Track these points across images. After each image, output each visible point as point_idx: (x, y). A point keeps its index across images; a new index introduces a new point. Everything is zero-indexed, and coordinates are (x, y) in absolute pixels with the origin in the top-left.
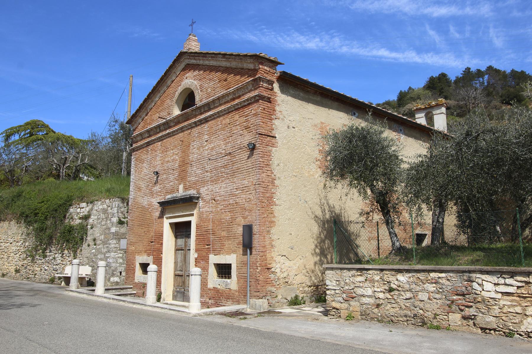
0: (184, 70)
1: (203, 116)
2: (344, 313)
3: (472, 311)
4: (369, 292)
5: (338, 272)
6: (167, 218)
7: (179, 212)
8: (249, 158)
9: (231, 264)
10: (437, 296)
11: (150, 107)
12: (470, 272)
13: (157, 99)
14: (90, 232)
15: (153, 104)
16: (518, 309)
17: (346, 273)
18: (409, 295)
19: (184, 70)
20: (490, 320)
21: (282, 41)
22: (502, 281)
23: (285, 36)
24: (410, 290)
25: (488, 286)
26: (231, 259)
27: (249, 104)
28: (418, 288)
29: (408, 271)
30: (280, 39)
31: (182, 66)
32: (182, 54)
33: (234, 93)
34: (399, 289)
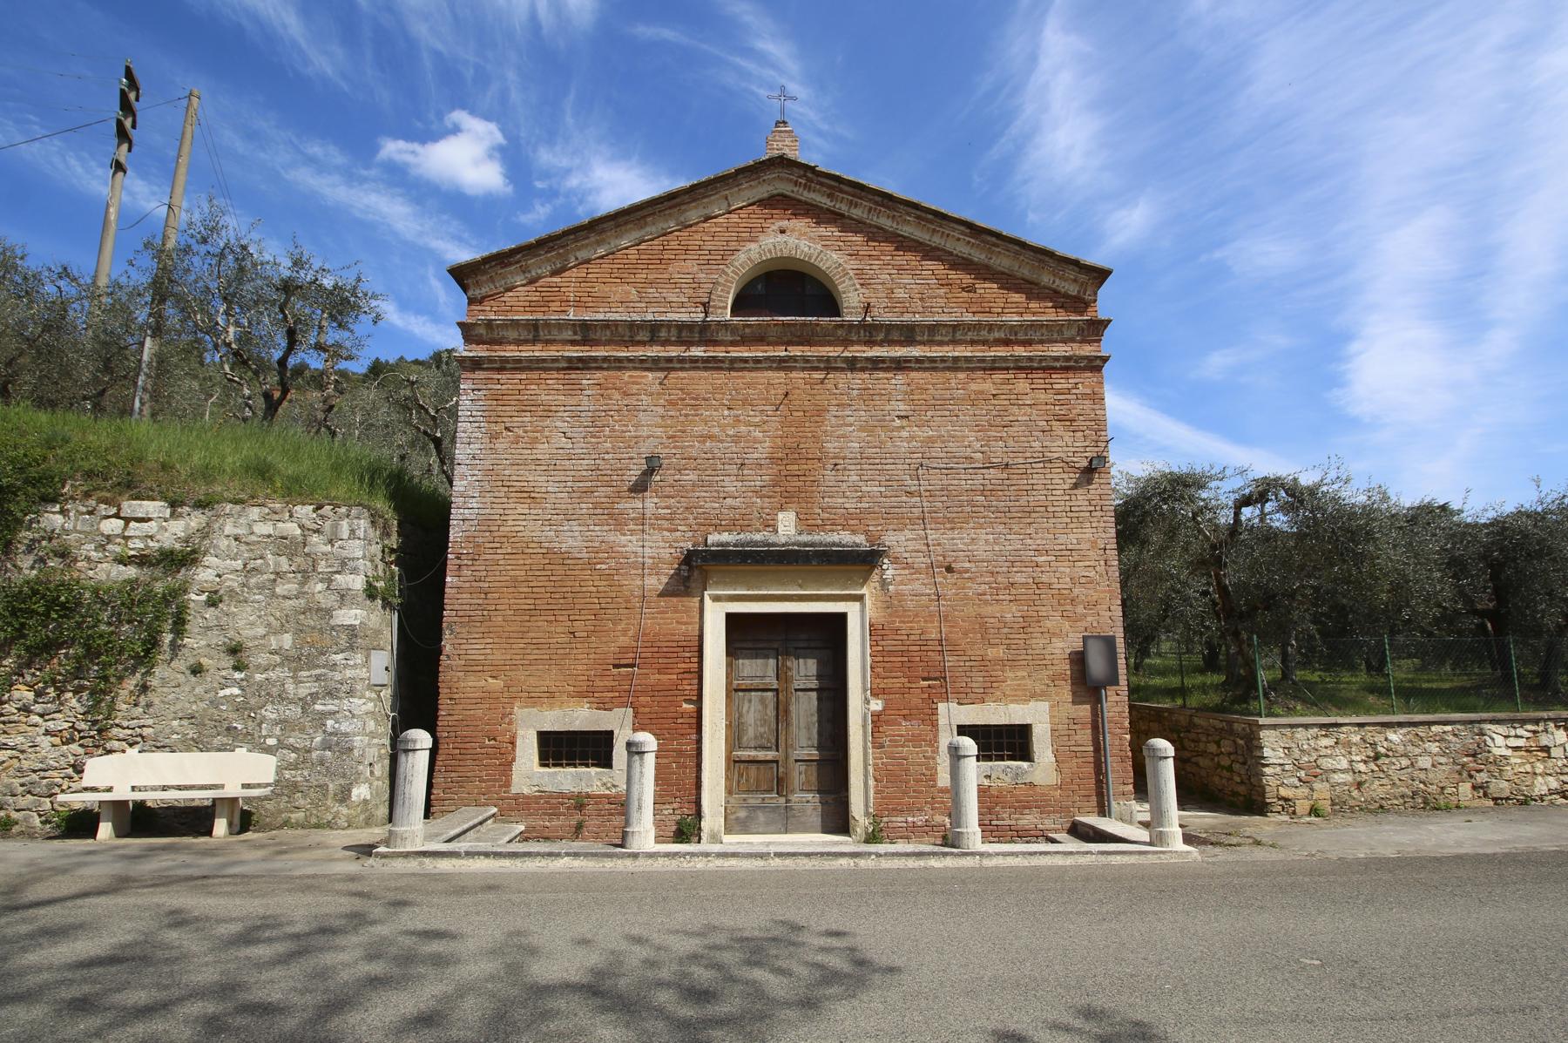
0: (762, 203)
2: (1302, 806)
3: (1481, 778)
4: (1344, 764)
5: (1287, 731)
6: (716, 599)
8: (1076, 486)
10: (1443, 760)
11: (582, 255)
12: (1479, 722)
13: (624, 243)
14: (200, 617)
15: (601, 251)
16: (1528, 768)
17: (1301, 734)
18: (1405, 762)
19: (762, 203)
20: (1501, 787)
21: (79, 170)
22: (1513, 733)
23: (93, 164)
24: (1405, 755)
25: (1500, 740)
26: (1037, 715)
27: (1067, 369)
28: (1417, 751)
29: (1401, 725)
30: (73, 162)
31: (763, 191)
32: (782, 162)
34: (1391, 752)
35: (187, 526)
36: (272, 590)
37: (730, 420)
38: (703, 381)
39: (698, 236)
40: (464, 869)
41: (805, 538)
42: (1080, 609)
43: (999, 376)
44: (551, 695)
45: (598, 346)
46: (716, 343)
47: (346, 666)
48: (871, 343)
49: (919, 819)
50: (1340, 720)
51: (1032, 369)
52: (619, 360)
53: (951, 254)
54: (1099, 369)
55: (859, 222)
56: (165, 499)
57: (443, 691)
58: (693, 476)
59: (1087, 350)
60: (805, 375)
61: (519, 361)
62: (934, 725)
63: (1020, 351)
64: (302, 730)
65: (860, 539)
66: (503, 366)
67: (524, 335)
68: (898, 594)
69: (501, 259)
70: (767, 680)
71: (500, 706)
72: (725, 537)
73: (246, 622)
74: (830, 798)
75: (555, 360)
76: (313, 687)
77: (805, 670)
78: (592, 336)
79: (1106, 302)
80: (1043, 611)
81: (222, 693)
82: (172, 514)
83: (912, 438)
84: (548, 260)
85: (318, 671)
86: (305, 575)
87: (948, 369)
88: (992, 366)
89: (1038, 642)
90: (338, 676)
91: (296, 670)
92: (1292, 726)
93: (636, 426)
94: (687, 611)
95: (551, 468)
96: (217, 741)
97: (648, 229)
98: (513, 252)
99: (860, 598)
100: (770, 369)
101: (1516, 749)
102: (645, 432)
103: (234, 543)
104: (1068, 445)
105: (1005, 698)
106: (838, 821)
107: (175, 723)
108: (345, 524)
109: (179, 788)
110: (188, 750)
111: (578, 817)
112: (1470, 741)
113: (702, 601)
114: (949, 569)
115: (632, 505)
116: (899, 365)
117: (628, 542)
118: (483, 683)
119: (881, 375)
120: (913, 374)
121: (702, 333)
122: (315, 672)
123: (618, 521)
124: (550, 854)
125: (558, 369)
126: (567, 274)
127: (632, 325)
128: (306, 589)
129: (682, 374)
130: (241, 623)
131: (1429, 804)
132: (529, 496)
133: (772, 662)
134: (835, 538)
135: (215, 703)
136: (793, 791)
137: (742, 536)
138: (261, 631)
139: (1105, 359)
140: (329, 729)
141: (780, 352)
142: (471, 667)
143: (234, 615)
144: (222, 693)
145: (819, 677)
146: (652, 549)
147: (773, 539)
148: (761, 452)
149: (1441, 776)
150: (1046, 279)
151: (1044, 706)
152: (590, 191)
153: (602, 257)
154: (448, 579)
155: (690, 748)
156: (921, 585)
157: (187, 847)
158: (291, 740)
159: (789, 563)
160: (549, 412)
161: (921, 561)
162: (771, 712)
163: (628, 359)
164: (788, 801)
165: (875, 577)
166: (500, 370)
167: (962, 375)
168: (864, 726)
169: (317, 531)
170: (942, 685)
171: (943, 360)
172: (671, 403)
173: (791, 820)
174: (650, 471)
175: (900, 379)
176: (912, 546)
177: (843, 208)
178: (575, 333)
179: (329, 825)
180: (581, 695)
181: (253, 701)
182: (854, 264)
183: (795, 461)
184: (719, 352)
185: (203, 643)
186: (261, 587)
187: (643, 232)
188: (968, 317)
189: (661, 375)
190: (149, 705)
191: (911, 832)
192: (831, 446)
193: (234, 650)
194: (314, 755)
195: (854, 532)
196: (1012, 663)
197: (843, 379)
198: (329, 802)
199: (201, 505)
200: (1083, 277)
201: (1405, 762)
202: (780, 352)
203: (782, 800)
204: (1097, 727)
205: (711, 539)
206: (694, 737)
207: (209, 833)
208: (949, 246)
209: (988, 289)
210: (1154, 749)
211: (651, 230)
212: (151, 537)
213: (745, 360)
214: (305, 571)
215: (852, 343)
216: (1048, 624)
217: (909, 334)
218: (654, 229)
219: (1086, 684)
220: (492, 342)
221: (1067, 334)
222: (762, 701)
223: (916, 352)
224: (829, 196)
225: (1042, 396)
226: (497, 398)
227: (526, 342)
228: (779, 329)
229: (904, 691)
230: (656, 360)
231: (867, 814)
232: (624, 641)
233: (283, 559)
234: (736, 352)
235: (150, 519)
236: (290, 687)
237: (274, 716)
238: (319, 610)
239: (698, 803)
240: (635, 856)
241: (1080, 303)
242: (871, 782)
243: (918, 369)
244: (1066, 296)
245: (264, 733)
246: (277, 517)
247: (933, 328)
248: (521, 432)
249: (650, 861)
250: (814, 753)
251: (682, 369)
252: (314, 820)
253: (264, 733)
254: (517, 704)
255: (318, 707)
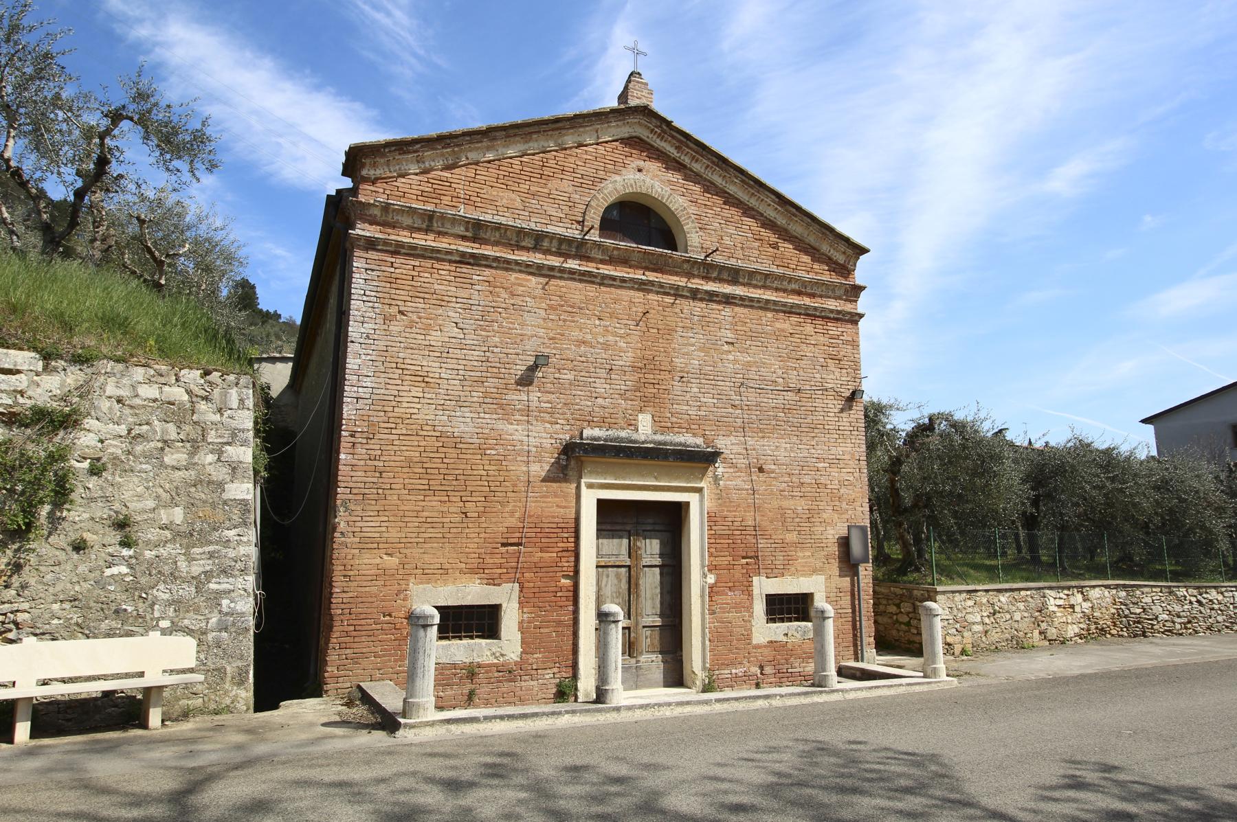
1: (711, 286)
3: (1044, 626)
4: (978, 619)
5: (950, 595)
6: (590, 486)
7: (677, 478)
8: (842, 411)
9: (812, 594)
11: (473, 156)
13: (511, 152)
14: (84, 486)
15: (490, 156)
17: (958, 597)
25: (1054, 600)
27: (837, 320)
29: (1006, 590)
31: (625, 131)
33: (804, 284)
35: (62, 385)
36: (160, 459)
37: (600, 330)
38: (577, 291)
39: (572, 160)
40: (488, 732)
41: (659, 437)
42: (844, 505)
43: (794, 319)
44: (444, 571)
45: (487, 244)
46: (588, 259)
47: (239, 543)
48: (707, 278)
49: (739, 671)
50: (978, 588)
51: (815, 316)
52: (508, 262)
53: (762, 215)
54: (856, 323)
55: (697, 174)
56: (35, 349)
57: (338, 569)
58: (570, 376)
59: (848, 307)
60: (659, 297)
61: (415, 248)
62: (750, 595)
63: (807, 301)
64: (197, 611)
65: (700, 441)
66: (397, 250)
67: (418, 223)
68: (726, 488)
69: (401, 147)
70: (621, 558)
71: (397, 580)
72: (597, 432)
73: (134, 494)
74: (669, 657)
75: (449, 253)
76: (208, 565)
77: (651, 549)
78: (482, 235)
79: (862, 272)
80: (822, 505)
81: (108, 572)
82: (45, 368)
83: (736, 361)
84: (443, 155)
85: (211, 548)
86: (195, 445)
87: (761, 308)
88: (790, 311)
89: (818, 529)
90: (231, 553)
91: (188, 547)
92: (953, 592)
93: (522, 325)
94: (565, 496)
95: (444, 355)
96: (104, 626)
97: (531, 144)
98: (415, 141)
99: (699, 490)
100: (632, 288)
101: (1059, 606)
102: (529, 331)
103: (117, 406)
104: (836, 379)
105: (797, 573)
106: (676, 676)
107: (56, 607)
108: (234, 392)
109: (64, 681)
110: (72, 636)
111: (469, 686)
112: (1038, 601)
113: (578, 488)
114: (761, 470)
115: (519, 397)
116: (728, 300)
117: (515, 431)
118: (378, 561)
119: (715, 306)
120: (737, 309)
121: (577, 249)
122: (207, 549)
123: (505, 410)
124: (553, 713)
125: (450, 261)
126: (456, 171)
127: (521, 232)
128: (196, 460)
129: (562, 283)
130: (127, 495)
131: (1019, 645)
132: (423, 380)
133: (625, 541)
134: (680, 439)
135: (100, 583)
136: (641, 653)
137: (610, 432)
138: (151, 504)
139: (861, 316)
140: (225, 609)
141: (639, 275)
142: (366, 544)
143: (120, 486)
144: (108, 572)
145: (661, 555)
146: (538, 440)
147: (635, 436)
148: (627, 358)
149: (1025, 625)
150: (825, 248)
151: (821, 579)
152: (156, 44)
153: (489, 162)
154: (342, 456)
155: (567, 618)
156: (741, 482)
157: (130, 742)
158: (186, 622)
159: (652, 459)
160: (442, 302)
161: (741, 462)
162: (624, 586)
163: (517, 263)
164: (638, 662)
165: (710, 473)
166: (395, 253)
167: (770, 315)
168: (702, 596)
169: (206, 398)
170: (755, 562)
171: (759, 300)
172: (551, 307)
173: (642, 678)
174: (533, 368)
175: (728, 311)
176: (736, 449)
177: (686, 160)
178: (467, 230)
179: (228, 710)
180: (473, 571)
181: (144, 580)
182: (693, 209)
183: (651, 371)
184: (590, 267)
185: (86, 516)
186: (148, 456)
187: (526, 146)
188: (774, 269)
189: (544, 280)
190: (24, 586)
191: (734, 682)
192: (679, 362)
193: (122, 525)
194: (210, 636)
195: (694, 435)
196: (799, 545)
197: (687, 306)
198: (227, 686)
199: (80, 360)
200: (849, 252)
201: (1008, 616)
202: (639, 275)
203: (633, 661)
204: (854, 594)
205: (586, 433)
206: (571, 608)
207: (144, 725)
208: (761, 209)
209: (787, 248)
210: (929, 610)
211: (533, 146)
212: (22, 393)
213: (613, 278)
214: (195, 441)
215: (694, 276)
216: (825, 516)
217: (734, 275)
218: (536, 145)
219: (848, 563)
220: (384, 224)
221: (838, 293)
222: (618, 576)
223: (739, 291)
224: (676, 148)
225: (822, 339)
226: (393, 281)
227: (419, 230)
228: (641, 255)
229: (730, 567)
230: (540, 267)
231: (704, 668)
232: (512, 522)
233: (171, 428)
234: (606, 270)
235: (18, 372)
236: (183, 565)
237: (166, 596)
238: (209, 483)
239: (575, 666)
240: (618, 709)
241: (845, 270)
242: (707, 642)
243: (741, 305)
244: (836, 263)
245: (157, 614)
246: (162, 380)
247: (752, 274)
248: (414, 317)
249: (630, 713)
250: (658, 621)
251: (561, 278)
252: (213, 706)
253: (157, 614)
254: (413, 580)
255: (212, 586)
